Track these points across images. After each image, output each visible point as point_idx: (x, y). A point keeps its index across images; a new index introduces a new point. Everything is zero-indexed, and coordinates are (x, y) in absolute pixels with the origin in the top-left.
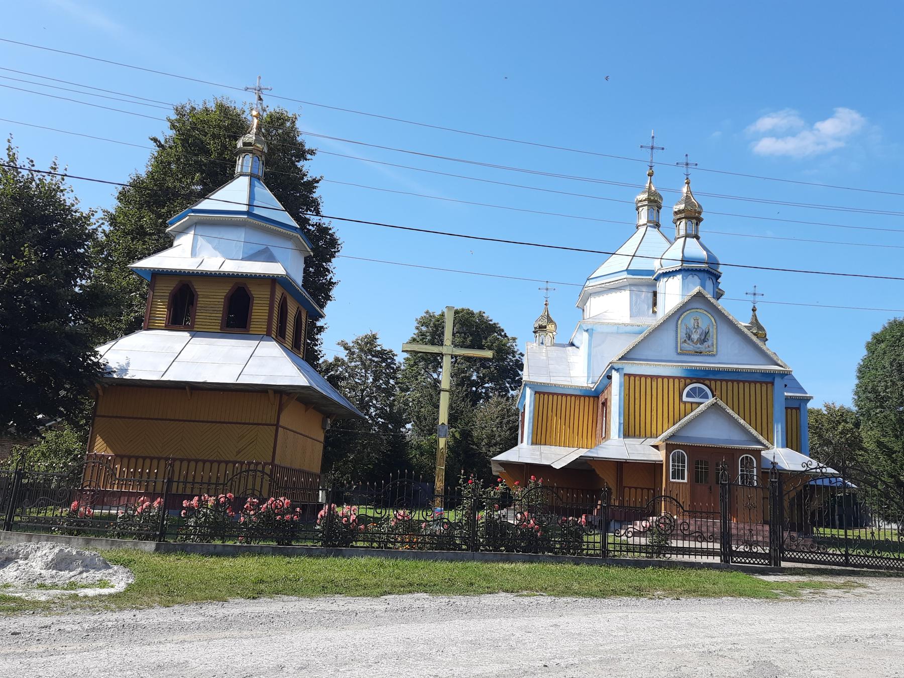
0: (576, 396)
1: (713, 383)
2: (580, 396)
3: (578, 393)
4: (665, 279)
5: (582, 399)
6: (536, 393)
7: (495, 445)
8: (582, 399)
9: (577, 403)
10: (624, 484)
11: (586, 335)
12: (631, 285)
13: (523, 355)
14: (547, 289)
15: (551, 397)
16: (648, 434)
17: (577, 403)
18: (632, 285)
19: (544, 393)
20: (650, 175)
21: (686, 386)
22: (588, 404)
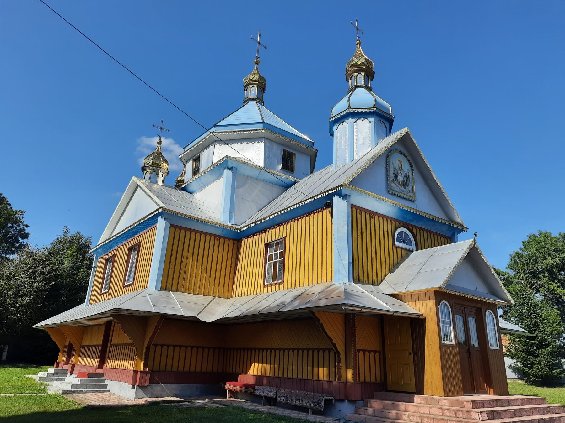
0: (215, 236)
1: (414, 229)
2: (220, 237)
3: (218, 232)
4: (354, 120)
5: (222, 240)
6: (171, 226)
7: (25, 295)
8: (222, 240)
9: (217, 244)
10: (358, 347)
11: (230, 173)
12: (265, 138)
13: (27, 226)
14: (161, 129)
15: (188, 233)
16: (370, 281)
17: (217, 244)
18: (265, 139)
19: (181, 228)
20: (257, 63)
21: (396, 229)
22: (226, 248)
